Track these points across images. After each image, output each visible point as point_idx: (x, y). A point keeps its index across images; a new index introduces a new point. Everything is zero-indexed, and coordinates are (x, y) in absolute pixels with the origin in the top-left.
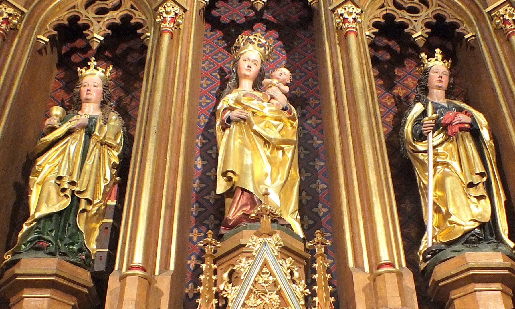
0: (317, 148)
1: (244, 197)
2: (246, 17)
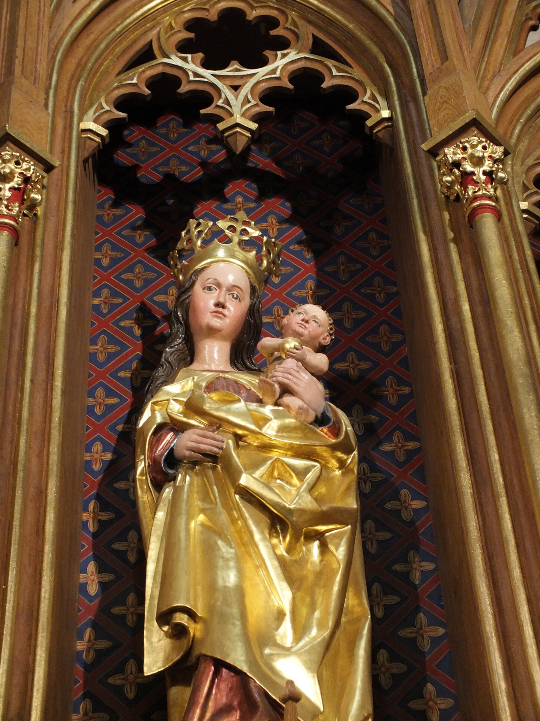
0: (412, 523)
1: (223, 686)
2: (203, 164)
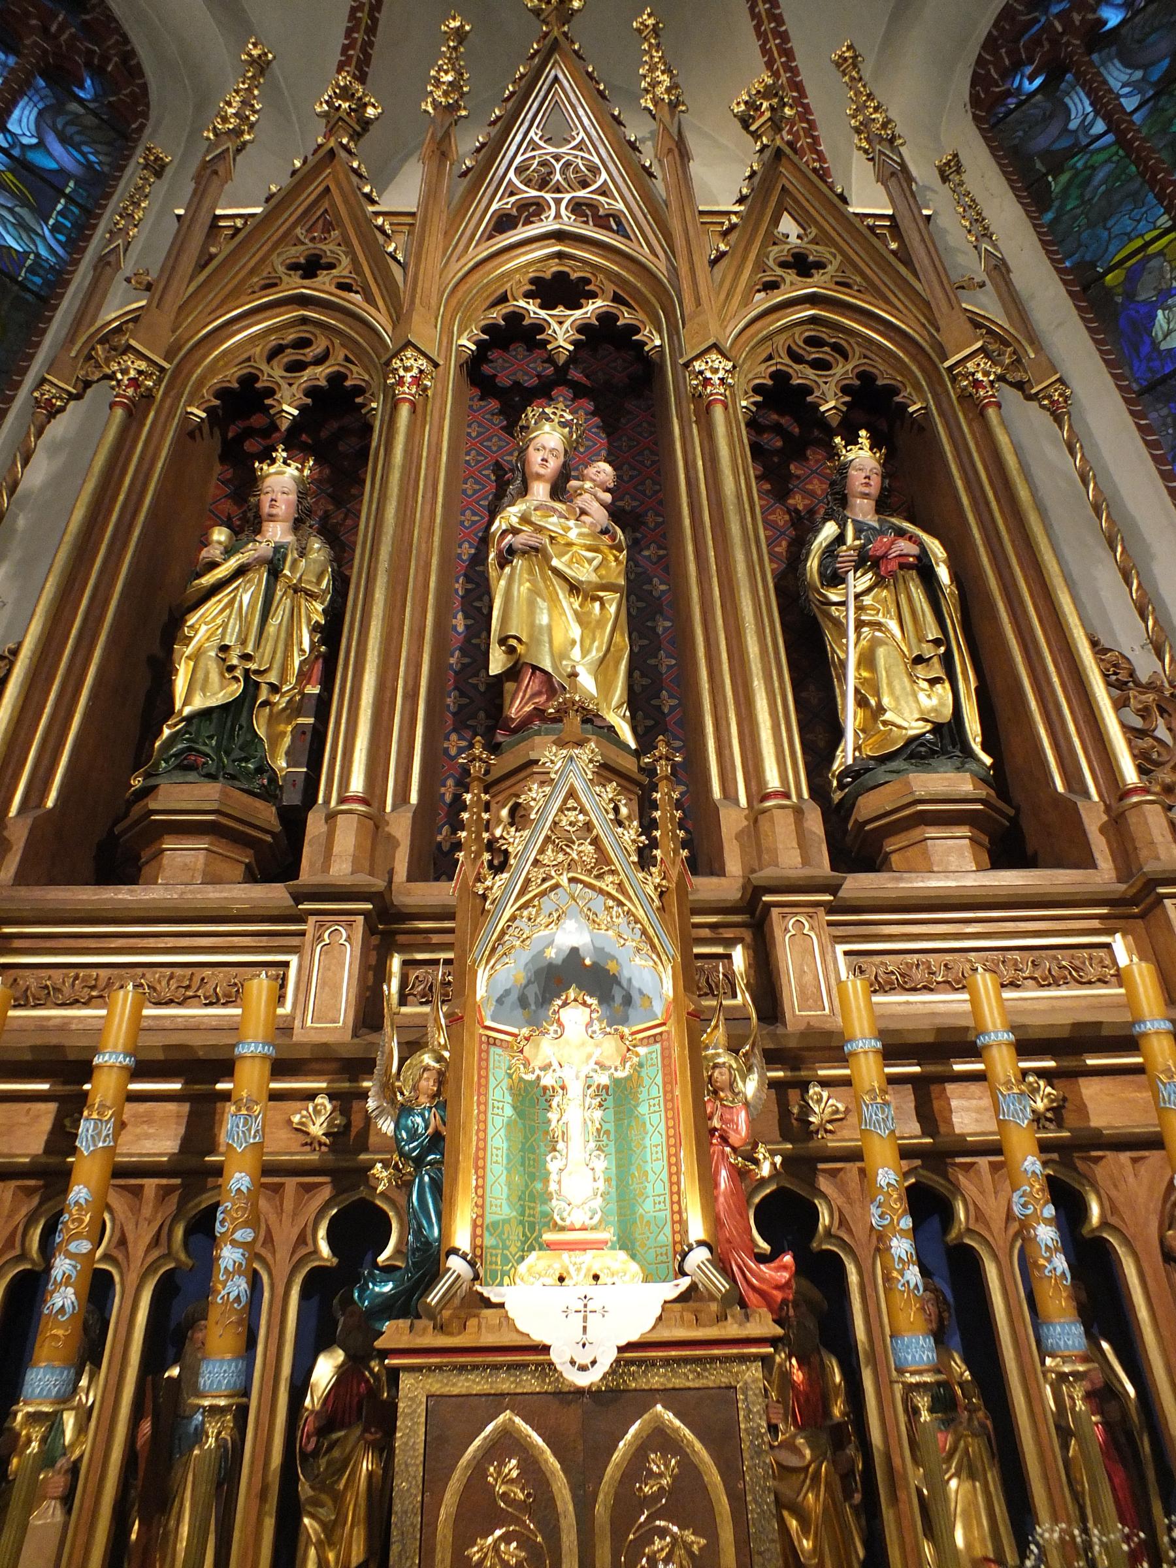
0: (660, 598)
2: (539, 376)
